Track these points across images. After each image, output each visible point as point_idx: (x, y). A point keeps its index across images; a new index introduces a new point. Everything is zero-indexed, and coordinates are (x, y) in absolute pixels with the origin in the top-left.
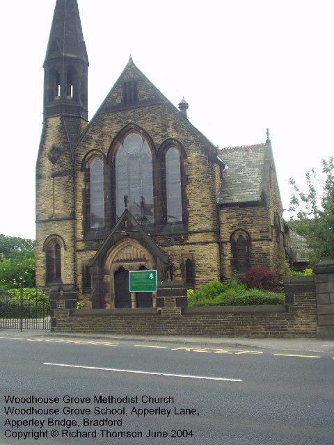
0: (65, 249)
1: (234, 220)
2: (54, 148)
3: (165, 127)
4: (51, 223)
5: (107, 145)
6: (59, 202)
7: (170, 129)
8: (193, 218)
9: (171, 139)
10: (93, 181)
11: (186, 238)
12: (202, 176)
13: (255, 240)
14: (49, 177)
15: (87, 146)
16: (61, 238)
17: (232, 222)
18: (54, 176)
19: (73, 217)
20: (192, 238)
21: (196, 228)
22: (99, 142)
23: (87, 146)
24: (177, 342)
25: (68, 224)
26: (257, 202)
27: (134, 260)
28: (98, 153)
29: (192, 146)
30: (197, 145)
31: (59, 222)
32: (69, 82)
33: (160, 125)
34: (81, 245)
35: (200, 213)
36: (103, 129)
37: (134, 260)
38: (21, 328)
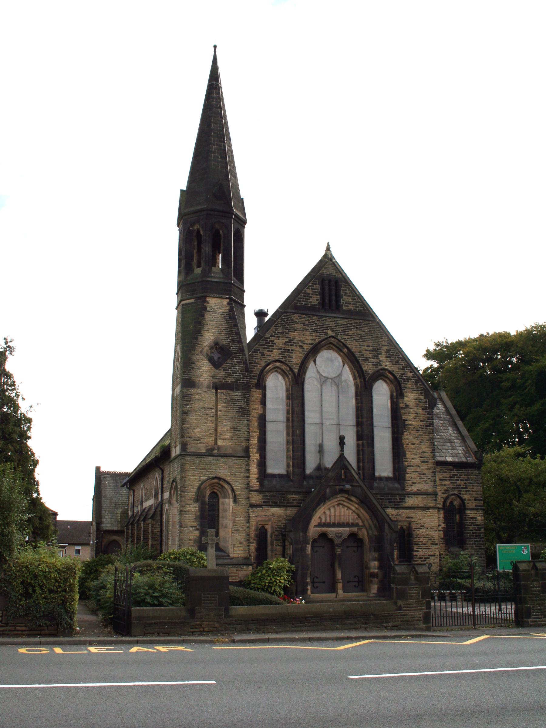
0: (235, 501)
1: (447, 483)
2: (216, 343)
3: (376, 352)
4: (211, 458)
5: (296, 359)
6: (225, 428)
7: (382, 357)
8: (411, 475)
9: (384, 369)
10: (269, 405)
11: (402, 500)
12: (421, 423)
13: (470, 509)
14: (208, 387)
15: (266, 352)
16: (228, 483)
17: (445, 485)
18: (216, 387)
19: (246, 454)
20: (410, 501)
21: (414, 488)
22: (284, 351)
23: (266, 352)
24: (348, 638)
25: (242, 463)
26: (265, 470)
27: (343, 525)
28: (284, 367)
29: (409, 385)
30: (416, 384)
31: (225, 459)
32: (216, 249)
33: (371, 348)
34: (256, 498)
35: (418, 469)
36: (292, 335)
37: (343, 525)
38: (474, 625)
